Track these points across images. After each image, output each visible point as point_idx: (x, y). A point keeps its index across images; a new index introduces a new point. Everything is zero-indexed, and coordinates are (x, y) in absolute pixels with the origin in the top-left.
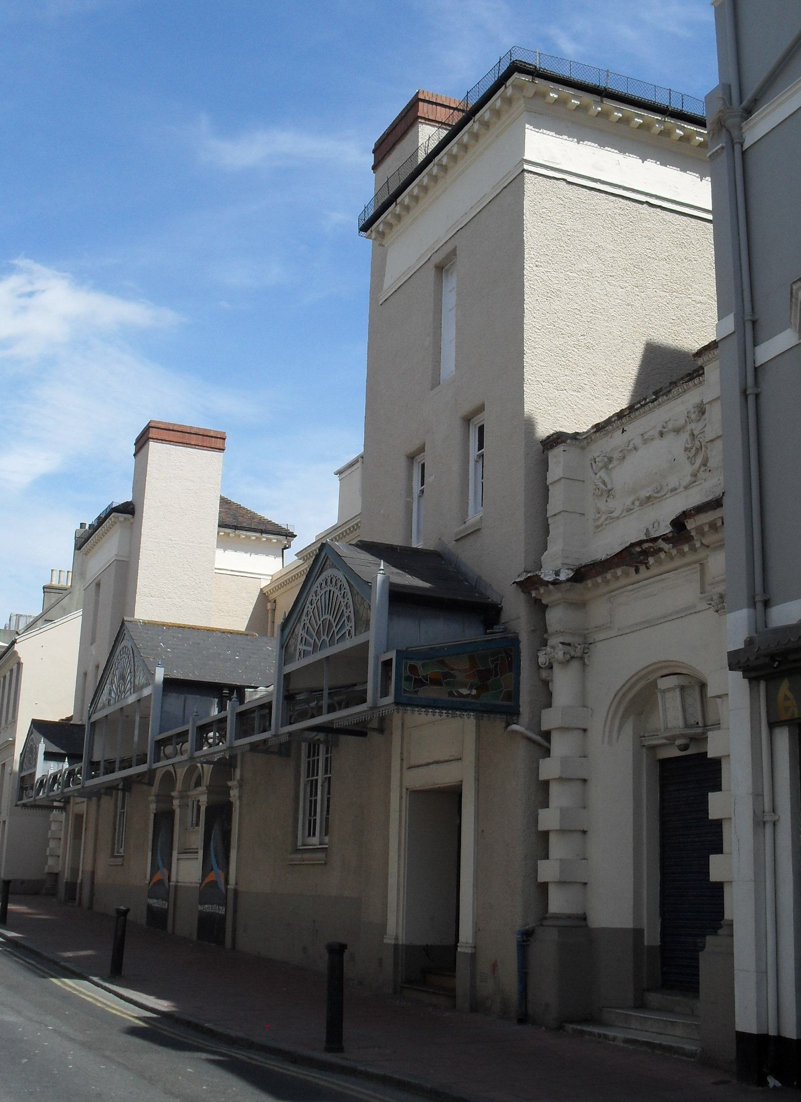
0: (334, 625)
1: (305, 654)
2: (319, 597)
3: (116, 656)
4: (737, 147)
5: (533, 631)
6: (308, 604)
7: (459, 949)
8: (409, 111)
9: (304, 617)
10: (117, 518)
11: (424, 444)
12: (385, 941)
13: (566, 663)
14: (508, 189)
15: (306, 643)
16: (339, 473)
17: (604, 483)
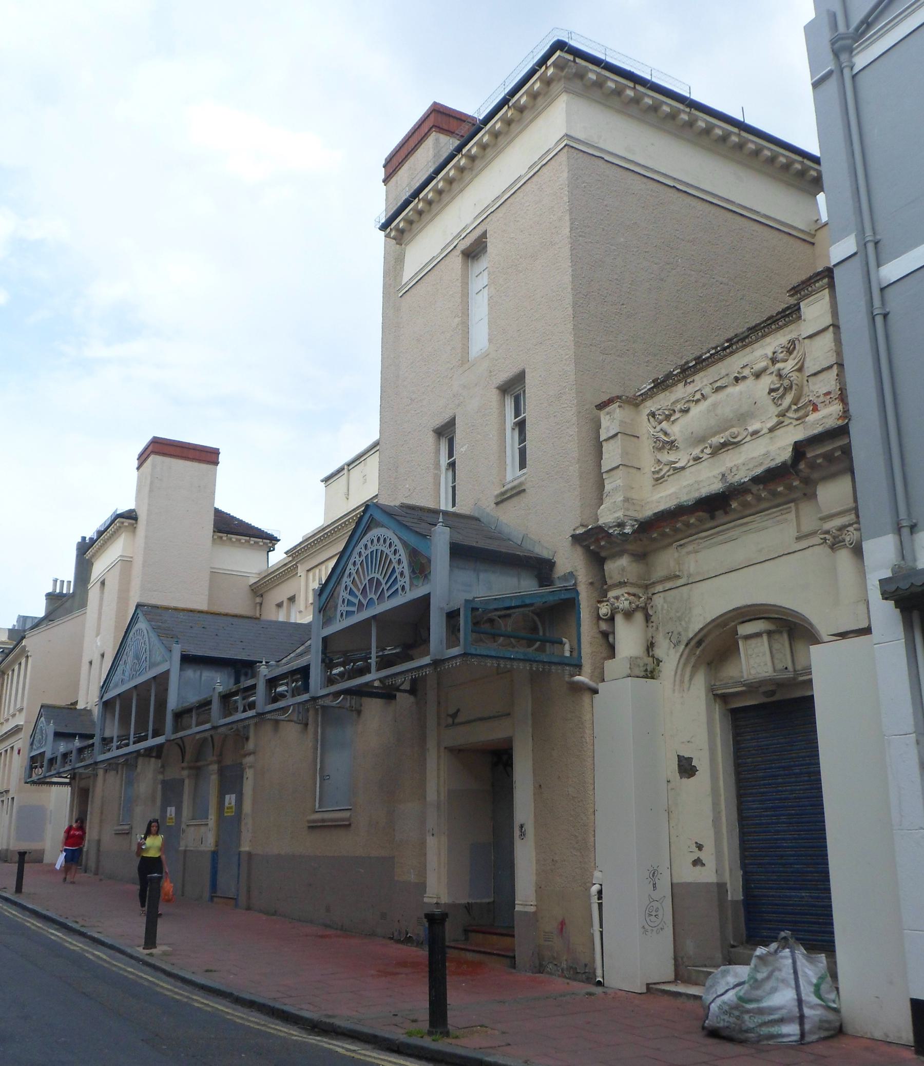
0: (383, 582)
1: (349, 613)
2: (363, 558)
3: (129, 639)
4: (846, 72)
5: (591, 584)
6: (350, 566)
7: (517, 908)
8: (413, 133)
9: (345, 579)
10: (123, 523)
11: (454, 418)
12: (426, 900)
13: (628, 615)
14: (547, 166)
15: (350, 603)
16: (326, 480)
17: (666, 434)
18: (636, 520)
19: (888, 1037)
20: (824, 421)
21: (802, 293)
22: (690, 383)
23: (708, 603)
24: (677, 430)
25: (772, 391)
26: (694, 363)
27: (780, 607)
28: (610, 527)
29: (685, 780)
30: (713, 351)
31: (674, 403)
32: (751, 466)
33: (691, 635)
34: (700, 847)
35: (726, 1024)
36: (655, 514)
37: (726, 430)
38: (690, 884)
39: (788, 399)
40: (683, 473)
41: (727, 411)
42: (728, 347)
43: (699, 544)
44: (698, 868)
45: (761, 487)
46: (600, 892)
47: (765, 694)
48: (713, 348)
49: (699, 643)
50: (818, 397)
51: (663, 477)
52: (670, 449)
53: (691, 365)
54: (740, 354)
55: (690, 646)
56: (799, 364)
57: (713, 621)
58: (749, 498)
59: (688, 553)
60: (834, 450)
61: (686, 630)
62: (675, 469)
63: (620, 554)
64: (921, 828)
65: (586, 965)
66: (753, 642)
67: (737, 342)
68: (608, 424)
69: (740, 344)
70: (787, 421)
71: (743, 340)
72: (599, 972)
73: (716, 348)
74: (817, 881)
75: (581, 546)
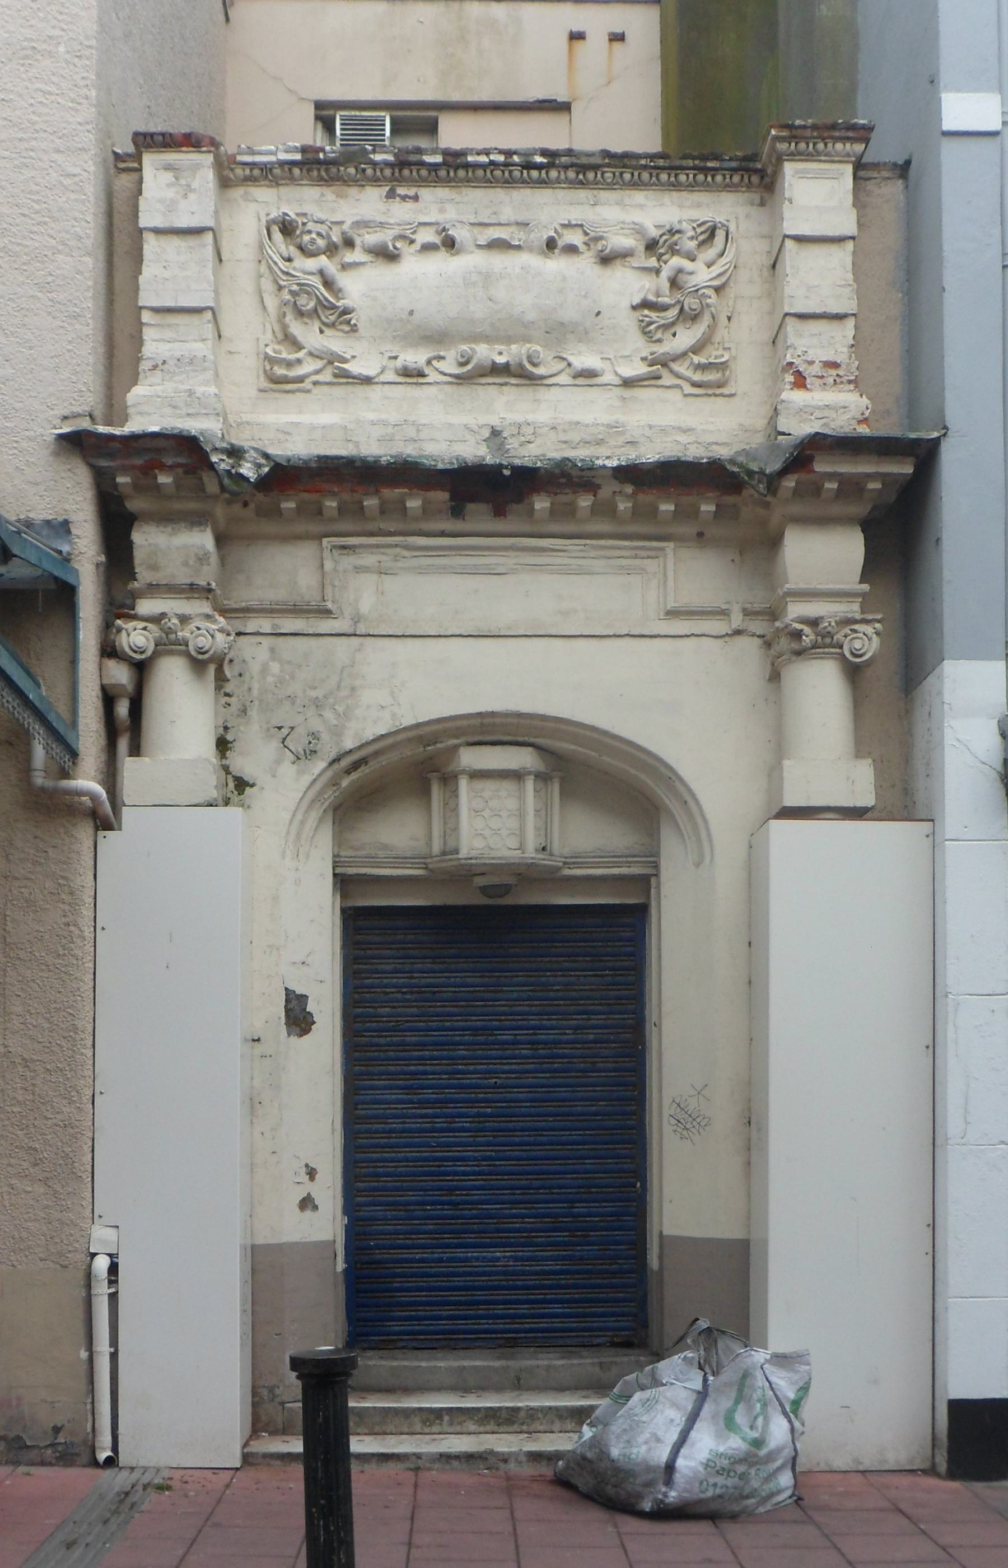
18: (266, 456)
19: (860, 1463)
20: (826, 413)
21: (802, 146)
22: (404, 198)
23: (400, 689)
24: (360, 285)
25: (646, 304)
26: (438, 159)
27: (605, 733)
28: (216, 449)
29: (294, 1039)
30: (501, 158)
31: (358, 224)
32: (575, 436)
33: (349, 744)
34: (312, 1173)
35: (718, 1491)
36: (322, 459)
37: (509, 340)
38: (296, 1243)
39: (685, 338)
40: (361, 390)
41: (525, 303)
42: (539, 167)
43: (396, 558)
44: (308, 1213)
45: (629, 489)
46: (113, 1269)
47: (484, 890)
48: (501, 152)
49: (355, 766)
50: (811, 363)
51: (300, 379)
52: (332, 326)
53: (428, 159)
54: (561, 194)
55: (336, 766)
56: (724, 279)
57: (418, 725)
58: (585, 502)
59: (358, 569)
60: (869, 476)
61: (337, 732)
62: (345, 374)
63: (196, 520)
64: (1003, 1143)
65: (57, 1430)
66: (488, 787)
67: (566, 167)
68: (170, 193)
69: (571, 174)
70: (667, 380)
71: (583, 168)
72: (105, 1439)
73: (508, 153)
74: (532, 1231)
75: (92, 466)
